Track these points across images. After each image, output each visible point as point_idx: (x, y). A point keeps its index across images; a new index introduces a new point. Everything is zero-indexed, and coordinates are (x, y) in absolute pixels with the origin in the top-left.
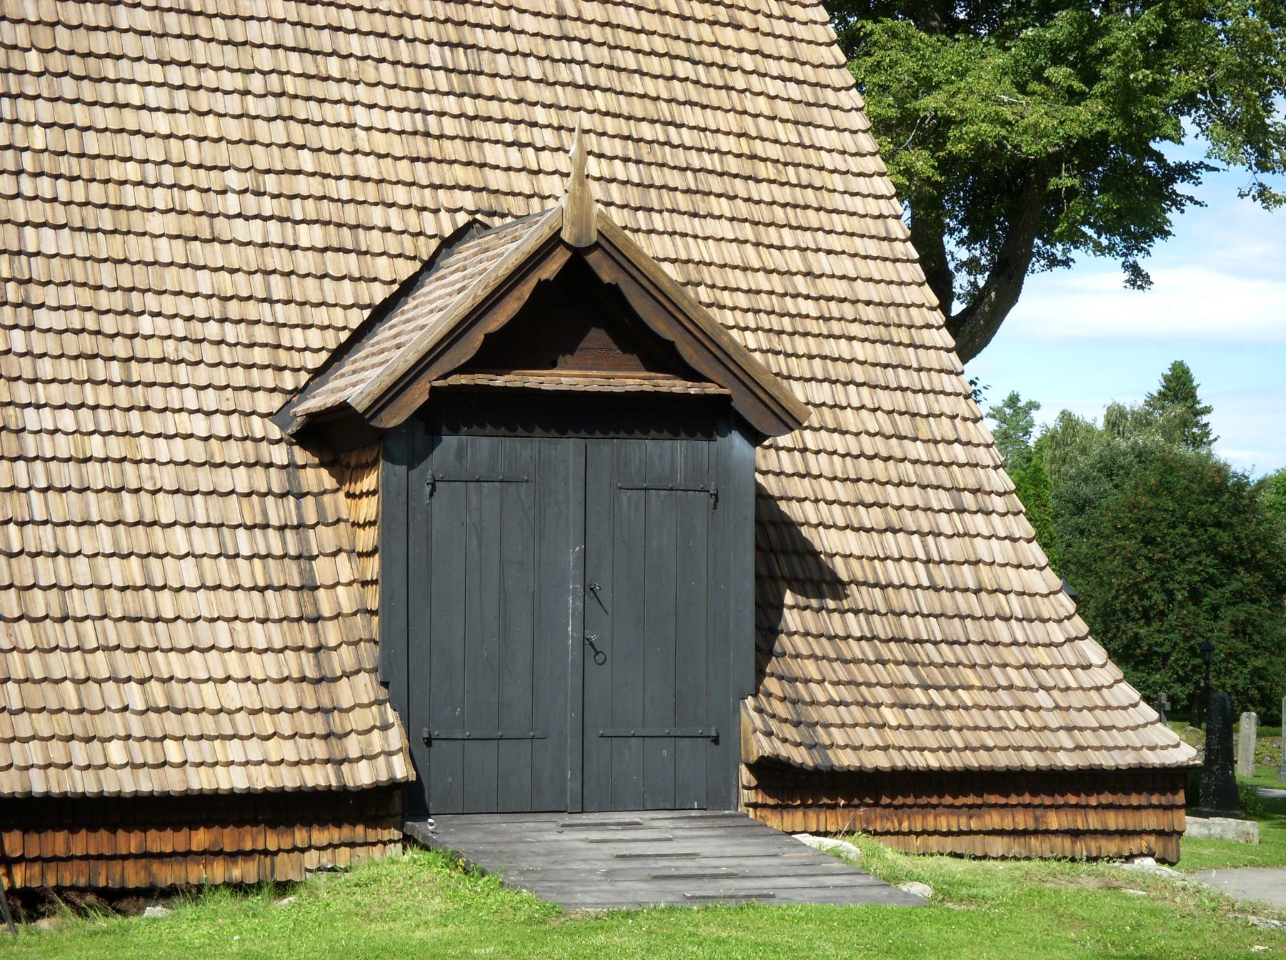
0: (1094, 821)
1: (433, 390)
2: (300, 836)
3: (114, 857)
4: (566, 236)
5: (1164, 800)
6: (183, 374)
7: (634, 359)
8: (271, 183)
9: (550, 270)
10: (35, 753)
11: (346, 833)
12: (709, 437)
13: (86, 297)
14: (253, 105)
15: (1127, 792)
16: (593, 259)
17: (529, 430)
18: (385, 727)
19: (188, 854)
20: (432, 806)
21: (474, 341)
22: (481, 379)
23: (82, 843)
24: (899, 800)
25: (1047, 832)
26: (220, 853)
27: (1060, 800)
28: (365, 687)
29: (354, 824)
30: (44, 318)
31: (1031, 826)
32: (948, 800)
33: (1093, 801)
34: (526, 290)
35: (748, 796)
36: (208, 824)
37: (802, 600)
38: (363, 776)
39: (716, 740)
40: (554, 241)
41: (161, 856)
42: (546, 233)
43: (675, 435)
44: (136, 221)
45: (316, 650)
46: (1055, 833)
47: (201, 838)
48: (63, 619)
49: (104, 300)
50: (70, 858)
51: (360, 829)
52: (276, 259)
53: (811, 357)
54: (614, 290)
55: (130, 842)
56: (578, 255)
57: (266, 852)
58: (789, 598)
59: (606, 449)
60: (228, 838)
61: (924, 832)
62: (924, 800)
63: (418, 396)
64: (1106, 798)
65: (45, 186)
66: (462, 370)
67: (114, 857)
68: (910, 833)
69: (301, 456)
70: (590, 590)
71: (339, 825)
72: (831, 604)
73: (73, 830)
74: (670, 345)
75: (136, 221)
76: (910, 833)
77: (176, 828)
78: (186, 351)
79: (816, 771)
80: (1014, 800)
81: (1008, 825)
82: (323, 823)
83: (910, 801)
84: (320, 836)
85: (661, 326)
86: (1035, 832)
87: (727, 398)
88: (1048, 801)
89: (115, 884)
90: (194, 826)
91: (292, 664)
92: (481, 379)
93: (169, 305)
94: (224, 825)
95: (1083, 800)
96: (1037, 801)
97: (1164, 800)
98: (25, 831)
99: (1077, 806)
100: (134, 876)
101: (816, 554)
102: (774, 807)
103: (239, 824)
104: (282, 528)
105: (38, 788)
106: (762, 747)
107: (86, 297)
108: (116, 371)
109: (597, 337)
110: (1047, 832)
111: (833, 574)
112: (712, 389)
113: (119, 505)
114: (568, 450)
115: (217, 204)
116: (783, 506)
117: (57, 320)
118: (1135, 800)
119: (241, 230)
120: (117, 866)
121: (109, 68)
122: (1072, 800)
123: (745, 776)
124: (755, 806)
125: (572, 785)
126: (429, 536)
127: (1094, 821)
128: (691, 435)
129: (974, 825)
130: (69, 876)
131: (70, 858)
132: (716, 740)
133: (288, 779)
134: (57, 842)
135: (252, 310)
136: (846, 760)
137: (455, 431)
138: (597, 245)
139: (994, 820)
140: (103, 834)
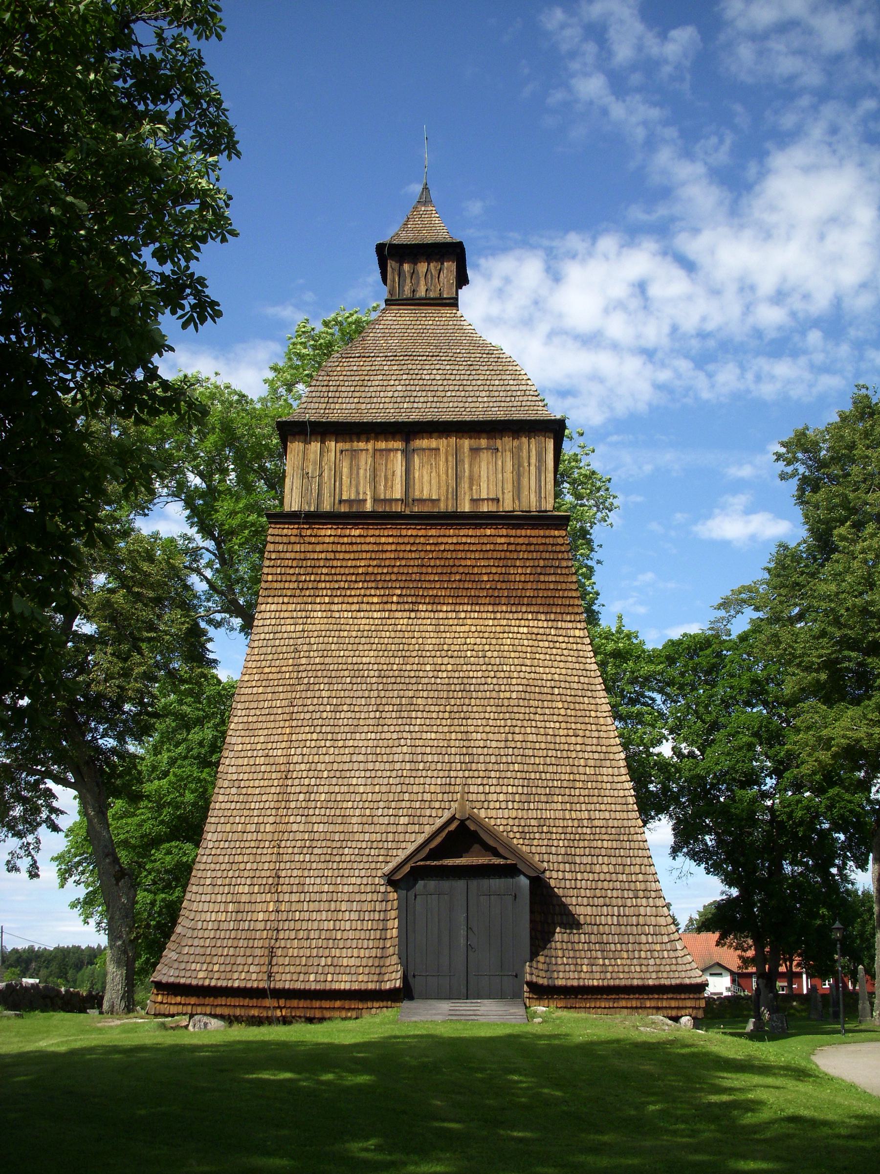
0: (665, 1004)
1: (412, 867)
2: (370, 1004)
3: (312, 1008)
4: (457, 816)
5: (696, 996)
6: (355, 865)
7: (490, 853)
8: (393, 805)
9: (453, 827)
10: (288, 977)
11: (385, 1004)
12: (512, 877)
13: (329, 844)
14: (391, 781)
15: (680, 993)
16: (467, 823)
17: (448, 878)
18: (397, 972)
19: (334, 1008)
20: (415, 996)
21: (426, 850)
22: (428, 863)
23: (302, 1004)
24: (585, 997)
25: (645, 1008)
26: (344, 1008)
27: (651, 996)
28: (395, 959)
29: (387, 1001)
30: (316, 851)
31: (639, 1005)
32: (605, 996)
33: (665, 997)
34: (444, 834)
35: (526, 994)
36: (340, 1000)
37: (563, 930)
38: (388, 986)
39: (516, 976)
40: (453, 818)
41: (326, 1008)
42: (450, 816)
43: (500, 877)
44: (348, 820)
45: (383, 948)
46: (649, 1008)
47: (338, 1004)
48: (307, 939)
49: (334, 844)
50: (299, 1008)
51: (389, 1003)
52: (392, 828)
53: (585, 848)
54: (475, 832)
55: (317, 1004)
56: (462, 822)
57: (358, 1009)
58: (558, 930)
59: (474, 883)
60: (347, 1004)
61: (595, 1007)
62: (595, 997)
63: (407, 869)
64: (670, 996)
65: (323, 811)
66: (421, 860)
67: (312, 1008)
68: (590, 1008)
69: (389, 889)
70: (468, 928)
71: (382, 1001)
72: (575, 931)
73: (300, 999)
74: (495, 848)
75: (348, 820)
76: (590, 1008)
77: (331, 1000)
78: (358, 859)
79: (548, 986)
80: (631, 996)
81: (629, 1005)
82: (377, 1000)
83: (589, 997)
84: (376, 1004)
85: (491, 843)
86: (641, 1008)
87: (516, 864)
88: (646, 997)
89: (312, 1016)
90: (336, 1000)
91: (374, 953)
92: (428, 863)
93: (354, 844)
94: (345, 1000)
95: (661, 996)
96: (641, 997)
97: (696, 996)
98: (286, 999)
99: (658, 998)
100: (318, 1014)
101: (573, 915)
102: (537, 999)
103: (350, 1000)
104: (380, 911)
105: (287, 987)
106: (528, 978)
107: (329, 844)
108: (335, 866)
109: (476, 847)
110: (645, 1008)
111: (578, 921)
112: (509, 862)
113: (330, 906)
114: (461, 884)
115: (375, 812)
116: (564, 899)
117: (319, 851)
118: (683, 996)
119: (382, 820)
120: (313, 1011)
121: (348, 774)
122: (656, 996)
123: (526, 988)
124: (529, 998)
125: (464, 991)
126: (414, 912)
127: (665, 1004)
128: (506, 877)
129: (615, 1005)
130: (298, 1013)
131: (299, 1008)
132: (516, 976)
133: (363, 987)
134: (295, 1003)
135: (380, 845)
136: (560, 982)
137: (422, 879)
138: (468, 818)
139: (623, 1003)
140: (309, 1001)
